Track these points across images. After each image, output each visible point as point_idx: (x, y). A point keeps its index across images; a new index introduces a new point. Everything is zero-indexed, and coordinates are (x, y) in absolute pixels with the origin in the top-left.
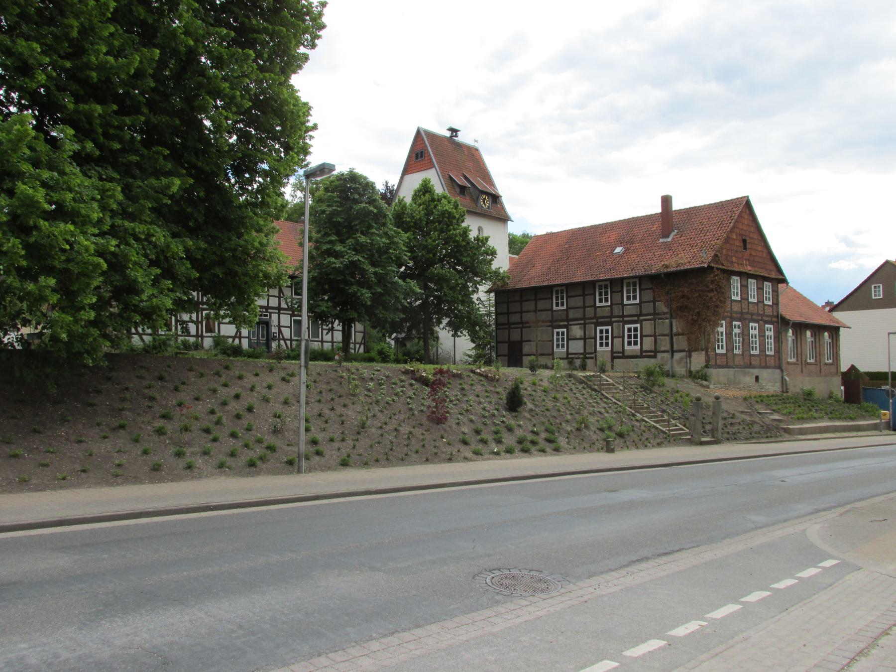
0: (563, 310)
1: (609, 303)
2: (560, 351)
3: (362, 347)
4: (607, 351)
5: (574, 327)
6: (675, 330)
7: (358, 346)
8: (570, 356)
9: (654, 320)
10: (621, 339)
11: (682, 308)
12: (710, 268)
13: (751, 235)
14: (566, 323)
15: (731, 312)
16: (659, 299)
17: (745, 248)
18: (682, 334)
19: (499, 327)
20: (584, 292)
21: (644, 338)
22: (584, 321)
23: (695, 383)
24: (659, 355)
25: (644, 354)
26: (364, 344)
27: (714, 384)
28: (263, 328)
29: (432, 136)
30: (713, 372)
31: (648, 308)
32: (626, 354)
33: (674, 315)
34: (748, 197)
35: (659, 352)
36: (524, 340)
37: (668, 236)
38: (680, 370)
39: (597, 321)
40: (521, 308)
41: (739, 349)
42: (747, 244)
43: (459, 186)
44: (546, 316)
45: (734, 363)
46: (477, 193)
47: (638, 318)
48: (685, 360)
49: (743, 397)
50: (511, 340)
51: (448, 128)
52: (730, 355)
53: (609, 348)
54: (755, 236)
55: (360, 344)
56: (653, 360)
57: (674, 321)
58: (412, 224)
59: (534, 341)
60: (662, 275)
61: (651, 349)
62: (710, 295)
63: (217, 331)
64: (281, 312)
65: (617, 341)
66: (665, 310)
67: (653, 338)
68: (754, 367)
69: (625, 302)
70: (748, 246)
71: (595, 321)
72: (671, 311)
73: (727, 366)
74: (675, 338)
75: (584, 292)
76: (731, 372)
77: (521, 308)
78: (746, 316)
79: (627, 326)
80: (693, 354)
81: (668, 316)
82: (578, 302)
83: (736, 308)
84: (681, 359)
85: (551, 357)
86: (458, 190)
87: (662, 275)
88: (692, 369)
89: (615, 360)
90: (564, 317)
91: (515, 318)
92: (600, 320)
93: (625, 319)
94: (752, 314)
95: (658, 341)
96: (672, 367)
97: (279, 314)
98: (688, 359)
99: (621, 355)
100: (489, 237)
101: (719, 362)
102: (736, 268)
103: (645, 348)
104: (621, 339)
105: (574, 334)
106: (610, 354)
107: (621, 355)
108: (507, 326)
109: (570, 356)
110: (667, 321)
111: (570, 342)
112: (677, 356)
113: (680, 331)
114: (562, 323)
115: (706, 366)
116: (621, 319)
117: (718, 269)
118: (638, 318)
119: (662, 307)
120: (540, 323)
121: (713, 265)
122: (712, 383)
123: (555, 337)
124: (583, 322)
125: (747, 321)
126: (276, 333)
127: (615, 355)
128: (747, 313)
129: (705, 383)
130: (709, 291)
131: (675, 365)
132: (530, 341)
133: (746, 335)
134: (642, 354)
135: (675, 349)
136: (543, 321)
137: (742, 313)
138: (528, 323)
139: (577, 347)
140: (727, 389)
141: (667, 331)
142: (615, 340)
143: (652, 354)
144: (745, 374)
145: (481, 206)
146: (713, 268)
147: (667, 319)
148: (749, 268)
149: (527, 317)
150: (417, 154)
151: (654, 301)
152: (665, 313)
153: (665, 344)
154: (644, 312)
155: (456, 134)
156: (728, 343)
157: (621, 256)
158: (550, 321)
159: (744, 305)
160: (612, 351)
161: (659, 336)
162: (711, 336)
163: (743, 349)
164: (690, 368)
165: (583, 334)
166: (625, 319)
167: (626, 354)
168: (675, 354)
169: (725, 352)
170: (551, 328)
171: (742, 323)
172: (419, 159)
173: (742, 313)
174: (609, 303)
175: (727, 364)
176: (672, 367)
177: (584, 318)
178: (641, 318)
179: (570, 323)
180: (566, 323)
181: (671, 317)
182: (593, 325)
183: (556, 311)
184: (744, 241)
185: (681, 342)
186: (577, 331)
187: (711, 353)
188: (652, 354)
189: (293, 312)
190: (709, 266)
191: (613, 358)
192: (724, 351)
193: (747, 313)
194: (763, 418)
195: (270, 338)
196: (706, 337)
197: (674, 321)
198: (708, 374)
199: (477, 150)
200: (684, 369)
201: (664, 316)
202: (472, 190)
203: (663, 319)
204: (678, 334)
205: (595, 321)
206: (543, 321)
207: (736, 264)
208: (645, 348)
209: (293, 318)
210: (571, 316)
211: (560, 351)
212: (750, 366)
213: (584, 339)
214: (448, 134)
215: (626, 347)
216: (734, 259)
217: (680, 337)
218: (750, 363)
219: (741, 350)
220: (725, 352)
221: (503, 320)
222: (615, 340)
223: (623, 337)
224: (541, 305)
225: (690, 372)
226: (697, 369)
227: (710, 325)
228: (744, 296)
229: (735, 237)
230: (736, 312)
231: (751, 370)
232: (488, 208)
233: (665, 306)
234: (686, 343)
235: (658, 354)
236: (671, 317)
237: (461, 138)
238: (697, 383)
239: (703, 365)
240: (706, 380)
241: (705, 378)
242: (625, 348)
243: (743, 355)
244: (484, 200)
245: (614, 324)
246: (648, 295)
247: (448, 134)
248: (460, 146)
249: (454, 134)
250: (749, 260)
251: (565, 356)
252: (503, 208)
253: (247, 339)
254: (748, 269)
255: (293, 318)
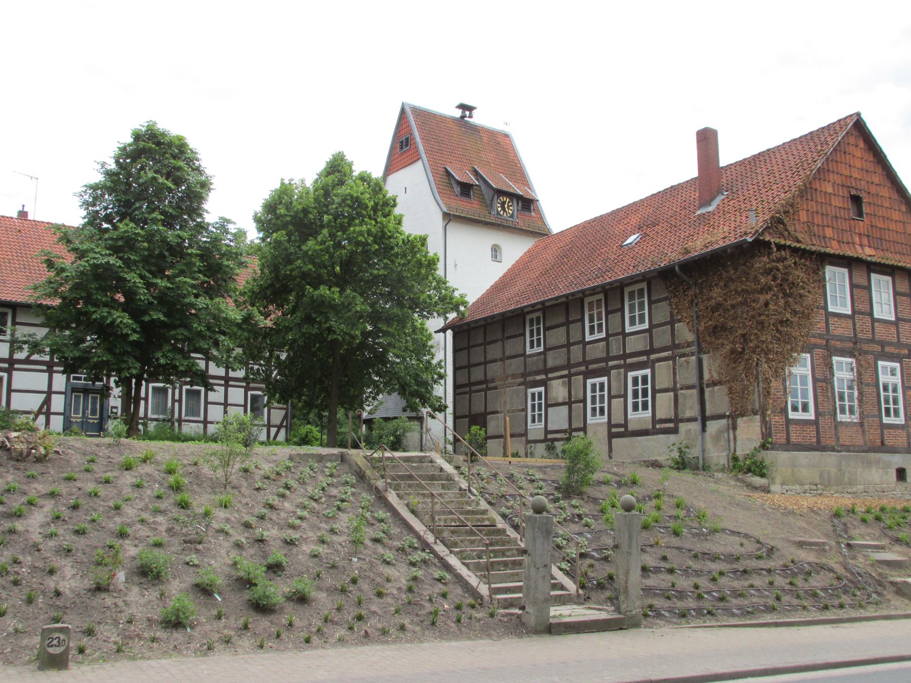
0: (539, 354)
1: (603, 335)
2: (535, 429)
3: (283, 432)
4: (601, 424)
5: (555, 383)
6: (706, 376)
7: (273, 430)
8: (549, 436)
9: (672, 358)
10: (622, 399)
11: (717, 330)
12: (759, 246)
13: (873, 190)
14: (543, 377)
15: (827, 336)
16: (679, 317)
17: (860, 214)
18: (720, 383)
19: (458, 391)
20: (567, 318)
21: (658, 395)
22: (569, 370)
23: (738, 480)
24: (683, 427)
25: (658, 426)
26: (286, 427)
27: (783, 484)
28: (94, 399)
29: (424, 116)
30: (779, 459)
31: (662, 337)
32: (631, 427)
33: (704, 345)
34: (858, 114)
35: (682, 421)
36: (488, 411)
37: (709, 203)
38: (718, 456)
39: (587, 368)
40: (485, 357)
41: (852, 412)
42: (863, 205)
43: (459, 183)
44: (515, 365)
45: (838, 439)
46: (491, 193)
47: (648, 358)
48: (726, 435)
49: (834, 509)
50: (473, 412)
51: (457, 104)
52: (825, 422)
53: (605, 419)
54: (886, 191)
55: (279, 427)
56: (672, 438)
57: (705, 357)
58: (288, 219)
59: (502, 413)
60: (677, 268)
61: (669, 417)
62: (763, 298)
63: (187, 418)
64: (231, 383)
65: (617, 403)
66: (690, 337)
67: (672, 394)
68: (893, 450)
69: (628, 329)
70: (866, 209)
71: (583, 368)
72: (698, 338)
73: (819, 447)
74: (707, 391)
75: (567, 318)
76: (830, 458)
77: (485, 357)
78: (866, 347)
79: (631, 375)
80: (740, 421)
81: (694, 348)
82: (558, 336)
83: (840, 329)
84: (720, 432)
85: (524, 438)
86: (457, 190)
87: (677, 268)
88: (739, 453)
89: (614, 440)
90: (541, 366)
91: (477, 374)
92: (592, 367)
93: (629, 361)
94: (883, 344)
95: (680, 400)
96: (703, 451)
97: (227, 386)
98: (731, 432)
99: (622, 430)
100: (427, 236)
101: (794, 438)
102: (834, 248)
103: (659, 416)
104: (622, 399)
105: (555, 395)
106: (606, 429)
107: (622, 430)
108: (467, 389)
109: (549, 436)
110: (694, 358)
111: (550, 410)
112: (713, 426)
113: (716, 377)
114: (538, 378)
115: (763, 447)
116: (622, 362)
117: (780, 247)
118: (648, 358)
119: (685, 333)
120: (510, 380)
121: (767, 239)
122: (778, 480)
123: (529, 402)
124: (566, 372)
125: (870, 357)
126: (116, 408)
127: (614, 430)
128: (873, 341)
129: (757, 480)
130: (761, 291)
131: (709, 445)
132: (497, 412)
133: (868, 385)
134: (657, 428)
135: (708, 413)
136: (514, 376)
137: (855, 341)
138: (493, 381)
139: (559, 418)
140: (820, 495)
141: (694, 380)
142: (581, 396)
143: (671, 425)
144: (869, 464)
145: (498, 213)
146: (768, 243)
147: (692, 354)
148: (868, 251)
149: (495, 370)
150: (402, 142)
151: (672, 323)
152: (689, 345)
153: (690, 408)
154: (657, 344)
155: (470, 113)
156: (820, 398)
157: (631, 247)
158: (523, 375)
159: (862, 323)
160: (610, 425)
161: (682, 389)
162: (774, 384)
163: (861, 414)
164: (735, 451)
165: (567, 395)
166: (629, 361)
167: (631, 427)
168: (708, 423)
169: (813, 417)
170: (523, 387)
171: (857, 360)
172: (404, 150)
173: (855, 341)
174: (603, 335)
175: (818, 441)
176: (703, 451)
177: (568, 366)
178: (653, 357)
179: (550, 375)
180: (543, 377)
181: (700, 350)
182: (581, 377)
183: (530, 356)
184: (856, 200)
185: (718, 399)
186: (559, 390)
187: (776, 420)
188: (671, 425)
189: (248, 383)
190: (756, 241)
191: (611, 436)
192: (811, 415)
193: (873, 341)
194: (854, 558)
195: (105, 416)
196: (761, 385)
197: (705, 357)
198: (767, 463)
199: (507, 136)
200: (725, 454)
201: (687, 350)
202: (483, 187)
203: (688, 355)
204: (714, 384)
205: (583, 368)
206: (514, 376)
207: (834, 243)
208: (659, 416)
209: (250, 393)
210: (550, 363)
211: (535, 429)
212: (883, 448)
213: (569, 403)
214: (458, 113)
215: (631, 415)
216: (829, 232)
217: (716, 388)
218: (882, 443)
219: (857, 415)
220: (813, 417)
221: (463, 380)
222: (614, 401)
223: (625, 396)
224: (512, 347)
225: (735, 459)
226: (748, 452)
227: (768, 361)
228: (860, 307)
229: (830, 190)
230: (841, 339)
231: (885, 457)
232: (512, 216)
233: (690, 331)
234: (727, 399)
235: (681, 425)
236: (700, 350)
237: (478, 119)
238: (742, 481)
239: (757, 444)
240: (762, 475)
241: (759, 469)
242: (629, 417)
243: (861, 424)
244: (503, 204)
245: (612, 372)
246: (663, 312)
247: (458, 113)
248: (476, 130)
249: (467, 113)
250: (868, 236)
251: (542, 437)
252: (541, 217)
253: (62, 417)
254: (868, 253)
255: (250, 393)
